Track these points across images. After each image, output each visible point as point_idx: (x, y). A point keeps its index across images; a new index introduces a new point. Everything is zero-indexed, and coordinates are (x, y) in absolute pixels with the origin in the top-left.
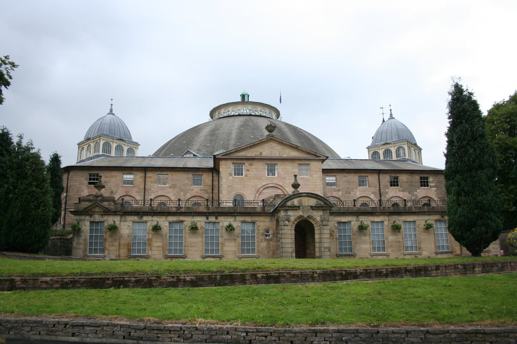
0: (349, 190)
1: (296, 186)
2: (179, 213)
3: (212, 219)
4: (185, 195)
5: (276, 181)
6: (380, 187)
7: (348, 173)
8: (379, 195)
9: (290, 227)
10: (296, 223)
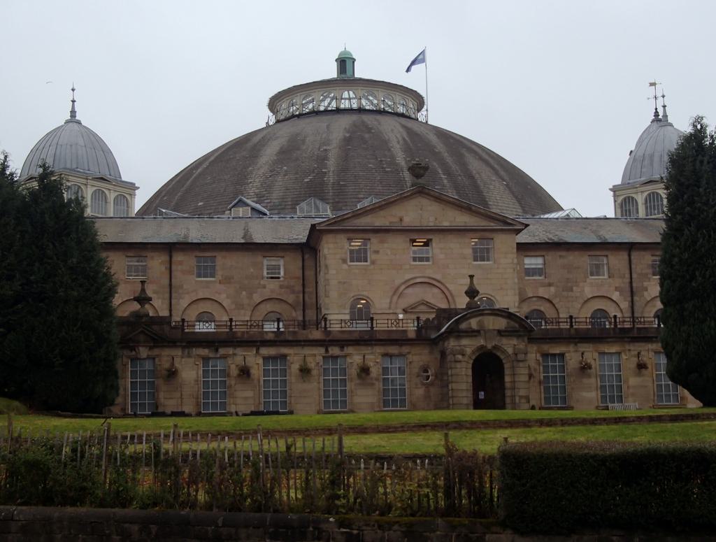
0: (570, 284)
1: (472, 293)
2: (280, 341)
3: (335, 351)
4: (250, 296)
5: (429, 273)
6: (631, 278)
7: (568, 250)
8: (629, 294)
9: (464, 364)
10: (474, 357)
